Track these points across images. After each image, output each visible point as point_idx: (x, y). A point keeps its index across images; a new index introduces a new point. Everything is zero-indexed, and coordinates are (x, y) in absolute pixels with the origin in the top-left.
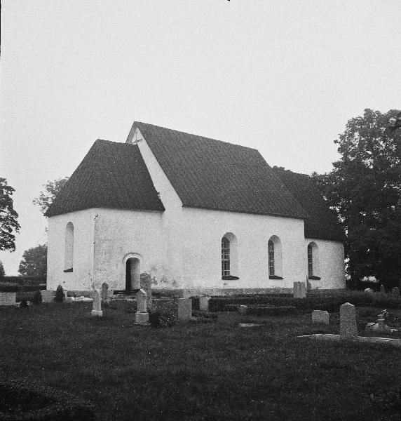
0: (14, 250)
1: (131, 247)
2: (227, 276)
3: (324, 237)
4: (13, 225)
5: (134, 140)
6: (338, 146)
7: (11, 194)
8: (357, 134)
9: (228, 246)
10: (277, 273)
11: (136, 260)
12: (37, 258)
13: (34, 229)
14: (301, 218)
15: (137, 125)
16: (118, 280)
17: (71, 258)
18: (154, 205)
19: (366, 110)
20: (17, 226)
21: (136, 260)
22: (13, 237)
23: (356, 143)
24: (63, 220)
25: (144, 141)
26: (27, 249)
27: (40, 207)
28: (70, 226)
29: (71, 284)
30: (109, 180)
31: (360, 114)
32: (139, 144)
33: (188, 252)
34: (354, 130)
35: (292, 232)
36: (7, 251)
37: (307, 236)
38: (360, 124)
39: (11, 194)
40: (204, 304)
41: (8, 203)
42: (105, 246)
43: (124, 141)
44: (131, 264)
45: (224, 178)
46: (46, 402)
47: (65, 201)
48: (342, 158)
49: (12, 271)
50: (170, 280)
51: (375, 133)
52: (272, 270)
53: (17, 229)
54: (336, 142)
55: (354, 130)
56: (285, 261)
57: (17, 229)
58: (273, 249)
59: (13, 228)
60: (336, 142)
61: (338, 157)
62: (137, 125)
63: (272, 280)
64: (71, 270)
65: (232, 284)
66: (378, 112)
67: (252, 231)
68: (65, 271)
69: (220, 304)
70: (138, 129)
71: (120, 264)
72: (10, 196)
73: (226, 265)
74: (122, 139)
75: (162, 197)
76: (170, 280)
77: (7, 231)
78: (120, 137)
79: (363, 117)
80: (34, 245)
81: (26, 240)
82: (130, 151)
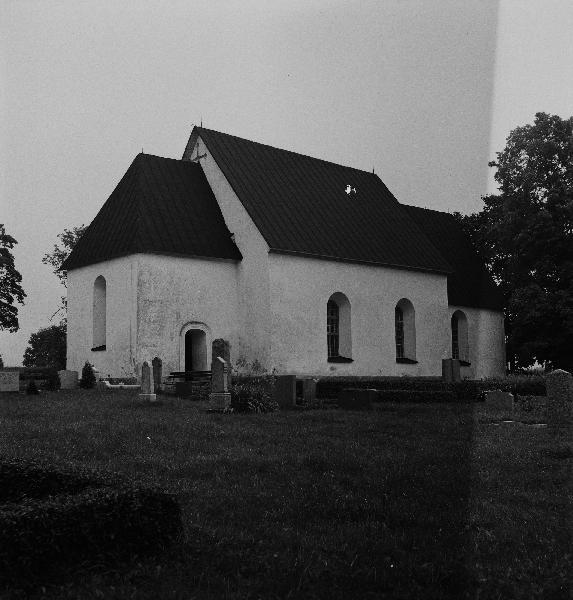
0: (16, 330)
1: (193, 312)
2: (335, 357)
3: (477, 304)
4: (14, 292)
5: (193, 157)
6: (495, 170)
7: (12, 247)
8: (524, 155)
9: (337, 312)
10: (407, 354)
11: (201, 334)
12: (50, 344)
13: (46, 297)
14: (444, 274)
15: (198, 132)
16: (174, 358)
17: (104, 335)
18: (225, 250)
19: (538, 115)
20: (21, 295)
21: (201, 334)
22: (15, 310)
23: (524, 165)
24: (86, 276)
25: (209, 156)
26: (36, 332)
27: (54, 268)
28: (101, 282)
29: (105, 368)
30: (158, 209)
31: (531, 121)
32: (202, 161)
33: (278, 310)
34: (520, 146)
35: (430, 294)
36: (6, 331)
37: (451, 303)
38: (529, 137)
39: (12, 247)
40: (310, 390)
41: (7, 260)
42: (153, 313)
43: (179, 157)
44: (193, 339)
45: (325, 209)
46: (79, 485)
47: (89, 248)
48: (501, 188)
49: (15, 358)
50: (250, 361)
51: (550, 150)
52: (400, 349)
53: (20, 299)
54: (492, 164)
55: (520, 146)
56: (420, 339)
57: (20, 299)
58: (402, 319)
59: (15, 297)
60: (492, 164)
61: (495, 189)
62: (198, 132)
63: (400, 365)
64: (102, 348)
65: (342, 370)
66: (556, 118)
67: (374, 291)
68: (93, 350)
69: (330, 389)
70: (200, 141)
71: (177, 338)
72: (10, 251)
73: (333, 340)
74: (177, 154)
75: (238, 240)
76: (250, 361)
77: (6, 302)
78: (173, 148)
79: (533, 125)
80: (47, 325)
81: (34, 317)
82: (188, 169)
